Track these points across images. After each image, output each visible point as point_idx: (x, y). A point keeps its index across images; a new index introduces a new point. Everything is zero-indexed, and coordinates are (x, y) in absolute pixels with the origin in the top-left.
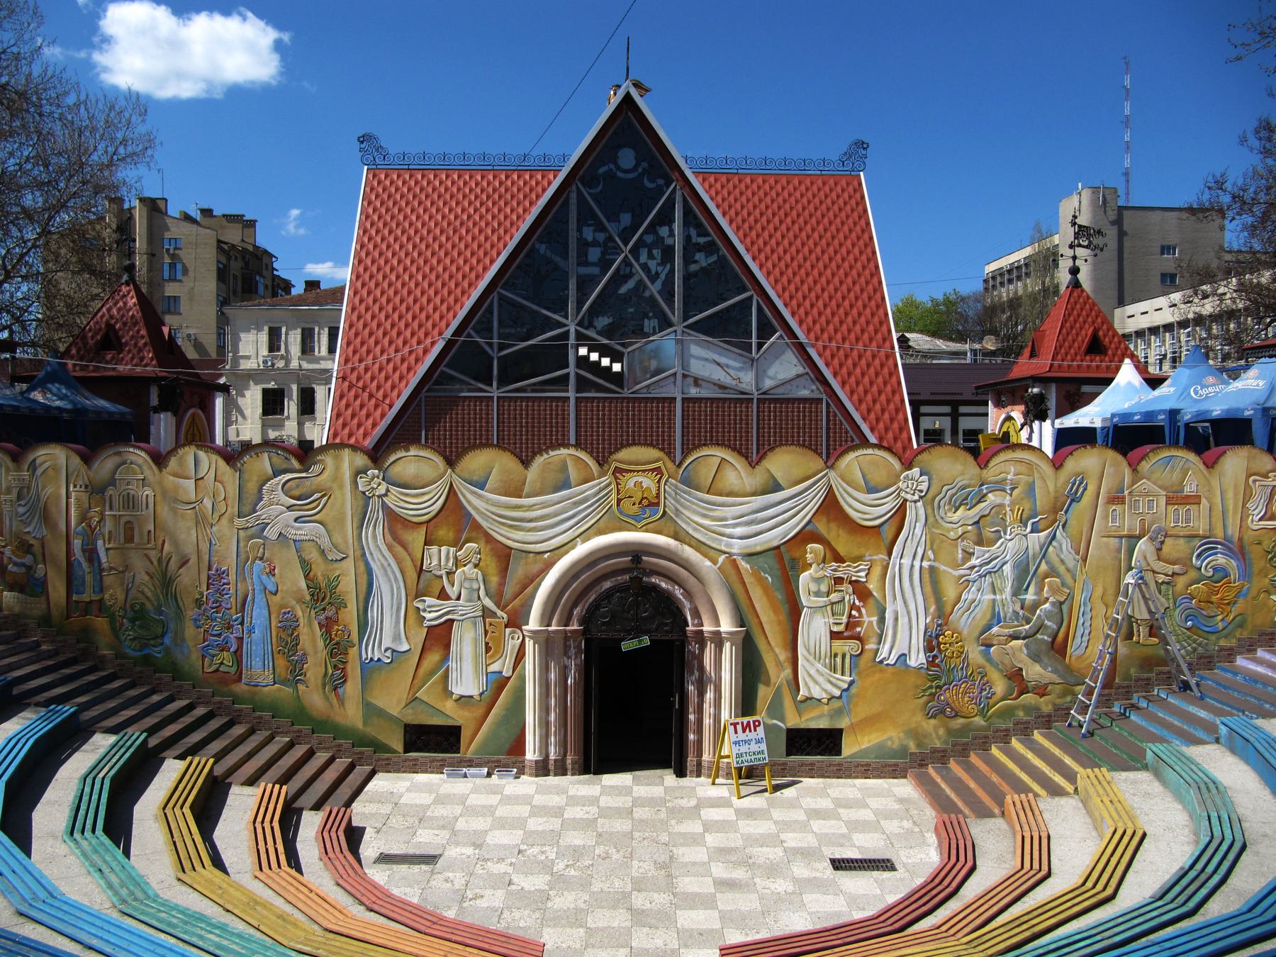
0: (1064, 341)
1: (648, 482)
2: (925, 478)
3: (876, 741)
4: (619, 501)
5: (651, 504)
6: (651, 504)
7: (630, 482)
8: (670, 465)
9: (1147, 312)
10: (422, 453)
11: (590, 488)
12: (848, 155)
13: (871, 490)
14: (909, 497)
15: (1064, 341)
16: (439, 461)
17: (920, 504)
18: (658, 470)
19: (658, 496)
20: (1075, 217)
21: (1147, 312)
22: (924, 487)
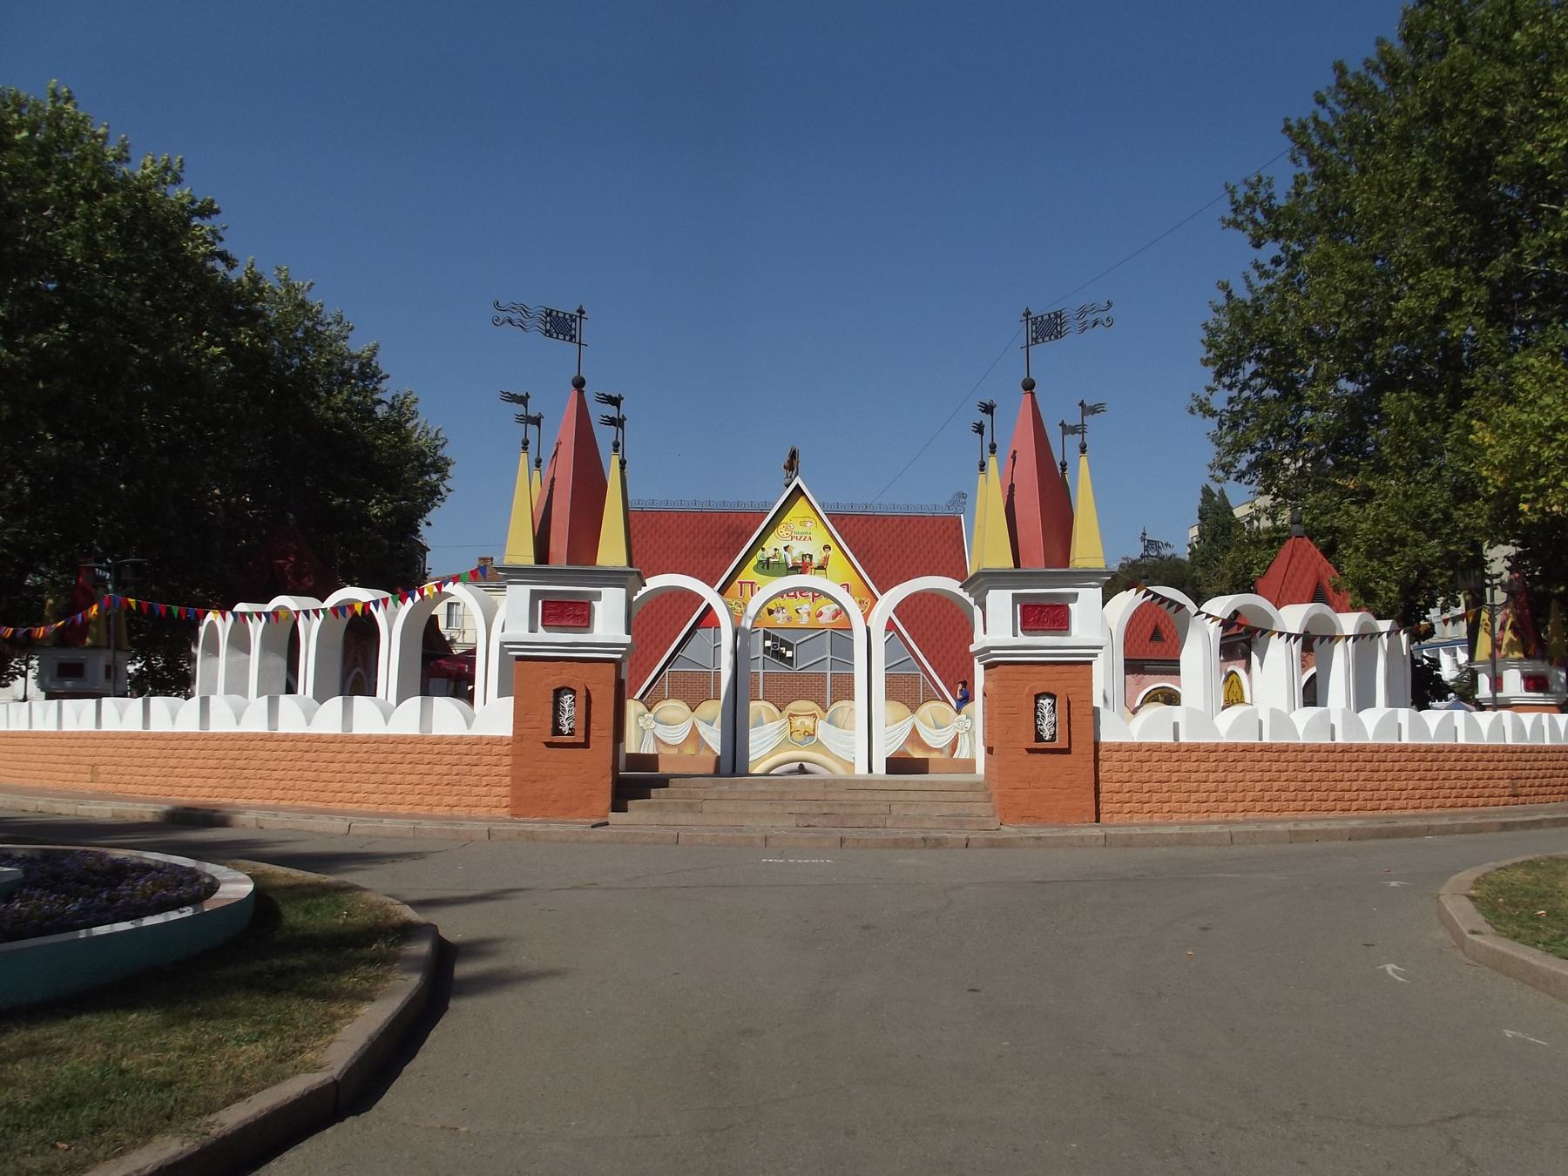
0: (1134, 631)
1: (808, 722)
2: (969, 720)
3: (55, 1030)
4: (791, 733)
5: (810, 735)
6: (810, 735)
7: (797, 722)
8: (822, 712)
9: (793, 455)
10: (677, 704)
11: (778, 723)
12: (952, 503)
13: (938, 727)
14: (960, 732)
15: (1134, 631)
16: (687, 708)
17: (966, 735)
18: (814, 716)
19: (814, 730)
20: (1144, 534)
21: (793, 455)
22: (969, 725)
